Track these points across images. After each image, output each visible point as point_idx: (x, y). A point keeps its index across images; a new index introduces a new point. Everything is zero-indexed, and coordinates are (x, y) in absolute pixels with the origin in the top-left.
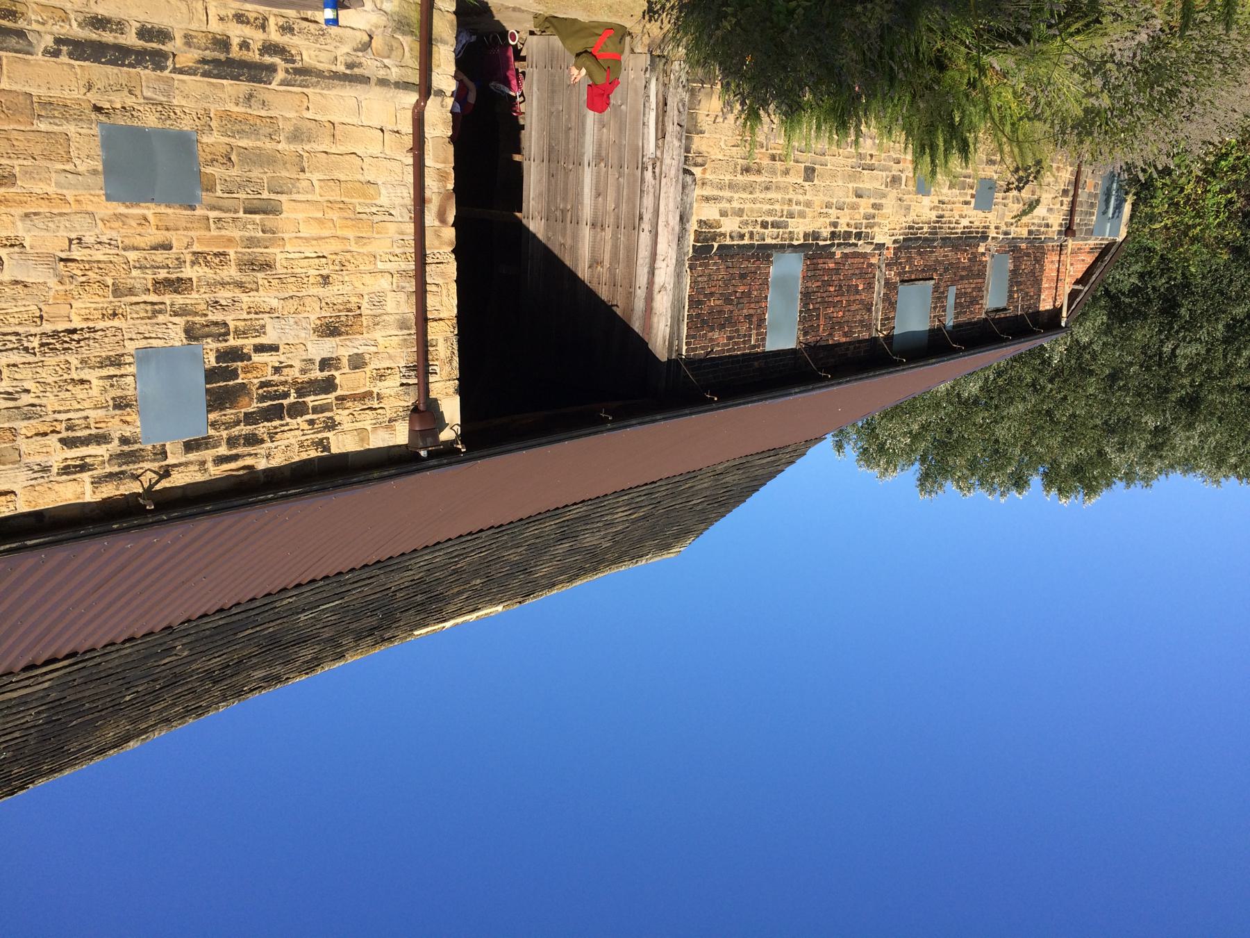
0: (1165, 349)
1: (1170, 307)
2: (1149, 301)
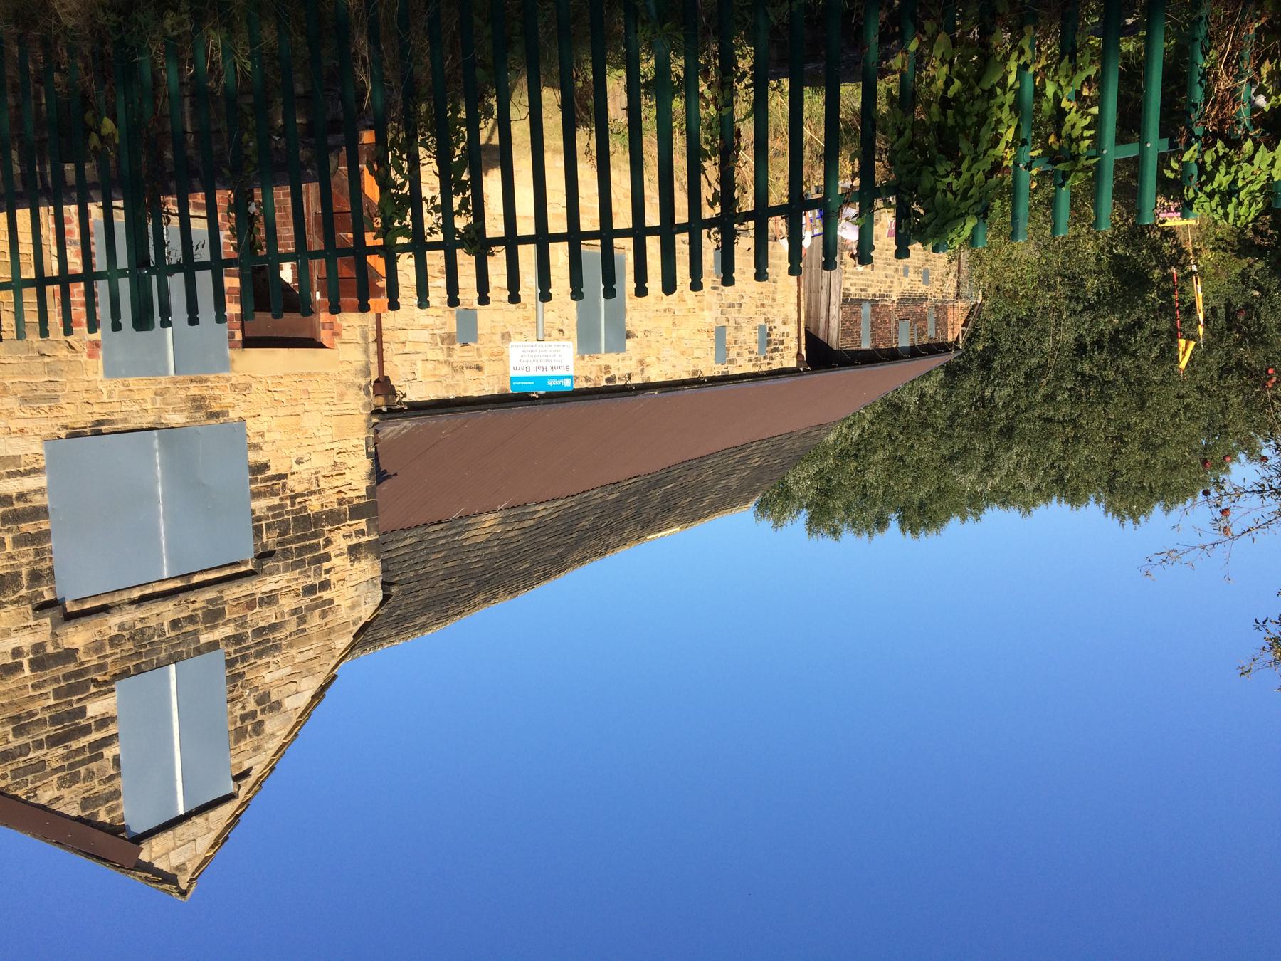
0: (986, 394)
1: (986, 364)
2: (971, 360)
